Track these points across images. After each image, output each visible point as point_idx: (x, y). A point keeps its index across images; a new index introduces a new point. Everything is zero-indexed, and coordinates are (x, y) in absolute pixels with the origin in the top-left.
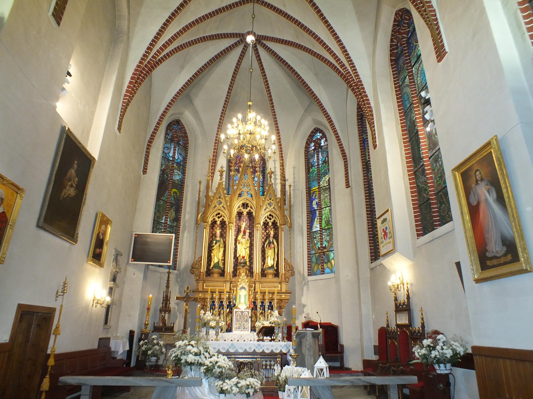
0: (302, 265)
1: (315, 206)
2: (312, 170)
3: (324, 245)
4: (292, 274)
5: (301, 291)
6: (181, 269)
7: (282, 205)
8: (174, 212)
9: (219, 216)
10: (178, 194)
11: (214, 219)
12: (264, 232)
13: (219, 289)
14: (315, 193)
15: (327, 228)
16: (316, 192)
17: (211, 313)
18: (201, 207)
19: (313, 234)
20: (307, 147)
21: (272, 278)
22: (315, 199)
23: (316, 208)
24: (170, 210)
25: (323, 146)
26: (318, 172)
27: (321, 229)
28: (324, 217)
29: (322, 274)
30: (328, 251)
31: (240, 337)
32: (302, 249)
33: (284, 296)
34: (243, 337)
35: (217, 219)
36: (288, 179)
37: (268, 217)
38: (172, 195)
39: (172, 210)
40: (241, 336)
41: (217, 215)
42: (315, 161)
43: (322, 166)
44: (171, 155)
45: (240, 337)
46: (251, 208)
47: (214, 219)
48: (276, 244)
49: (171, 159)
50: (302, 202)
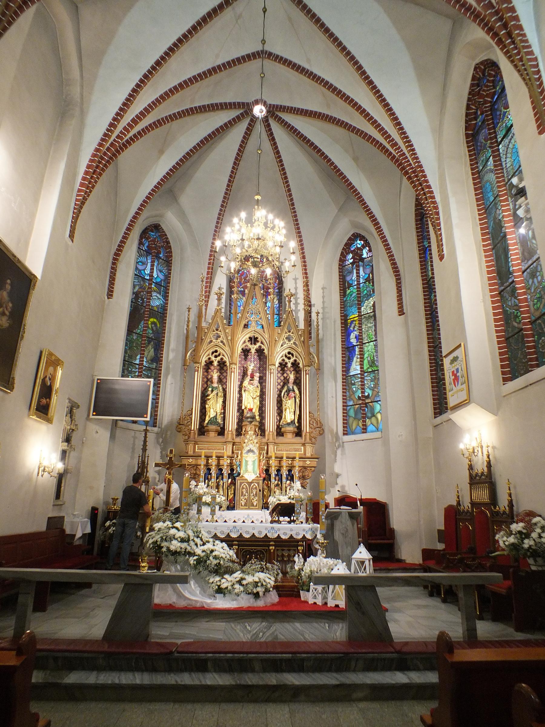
0: (335, 421)
1: (354, 341)
2: (349, 291)
3: (366, 394)
4: (321, 433)
5: (333, 456)
6: (163, 426)
7: (306, 340)
8: (153, 349)
9: (217, 354)
10: (158, 326)
11: (209, 359)
12: (281, 376)
13: (216, 453)
14: (354, 322)
15: (371, 370)
16: (355, 321)
17: (205, 484)
18: (190, 343)
19: (351, 378)
20: (342, 260)
21: (293, 438)
22: (354, 330)
23: (355, 344)
24: (147, 346)
25: (365, 258)
26: (357, 294)
27: (363, 372)
28: (366, 356)
29: (363, 433)
30: (372, 402)
31: (246, 517)
32: (334, 399)
33: (309, 462)
34: (251, 517)
35: (213, 358)
36: (314, 304)
37: (286, 356)
38: (150, 326)
39: (150, 347)
40: (248, 516)
41: (213, 353)
42: (353, 278)
43: (363, 286)
44: (148, 271)
45: (246, 517)
46: (262, 343)
47: (209, 359)
48: (297, 391)
49: (148, 278)
50: (335, 335)
